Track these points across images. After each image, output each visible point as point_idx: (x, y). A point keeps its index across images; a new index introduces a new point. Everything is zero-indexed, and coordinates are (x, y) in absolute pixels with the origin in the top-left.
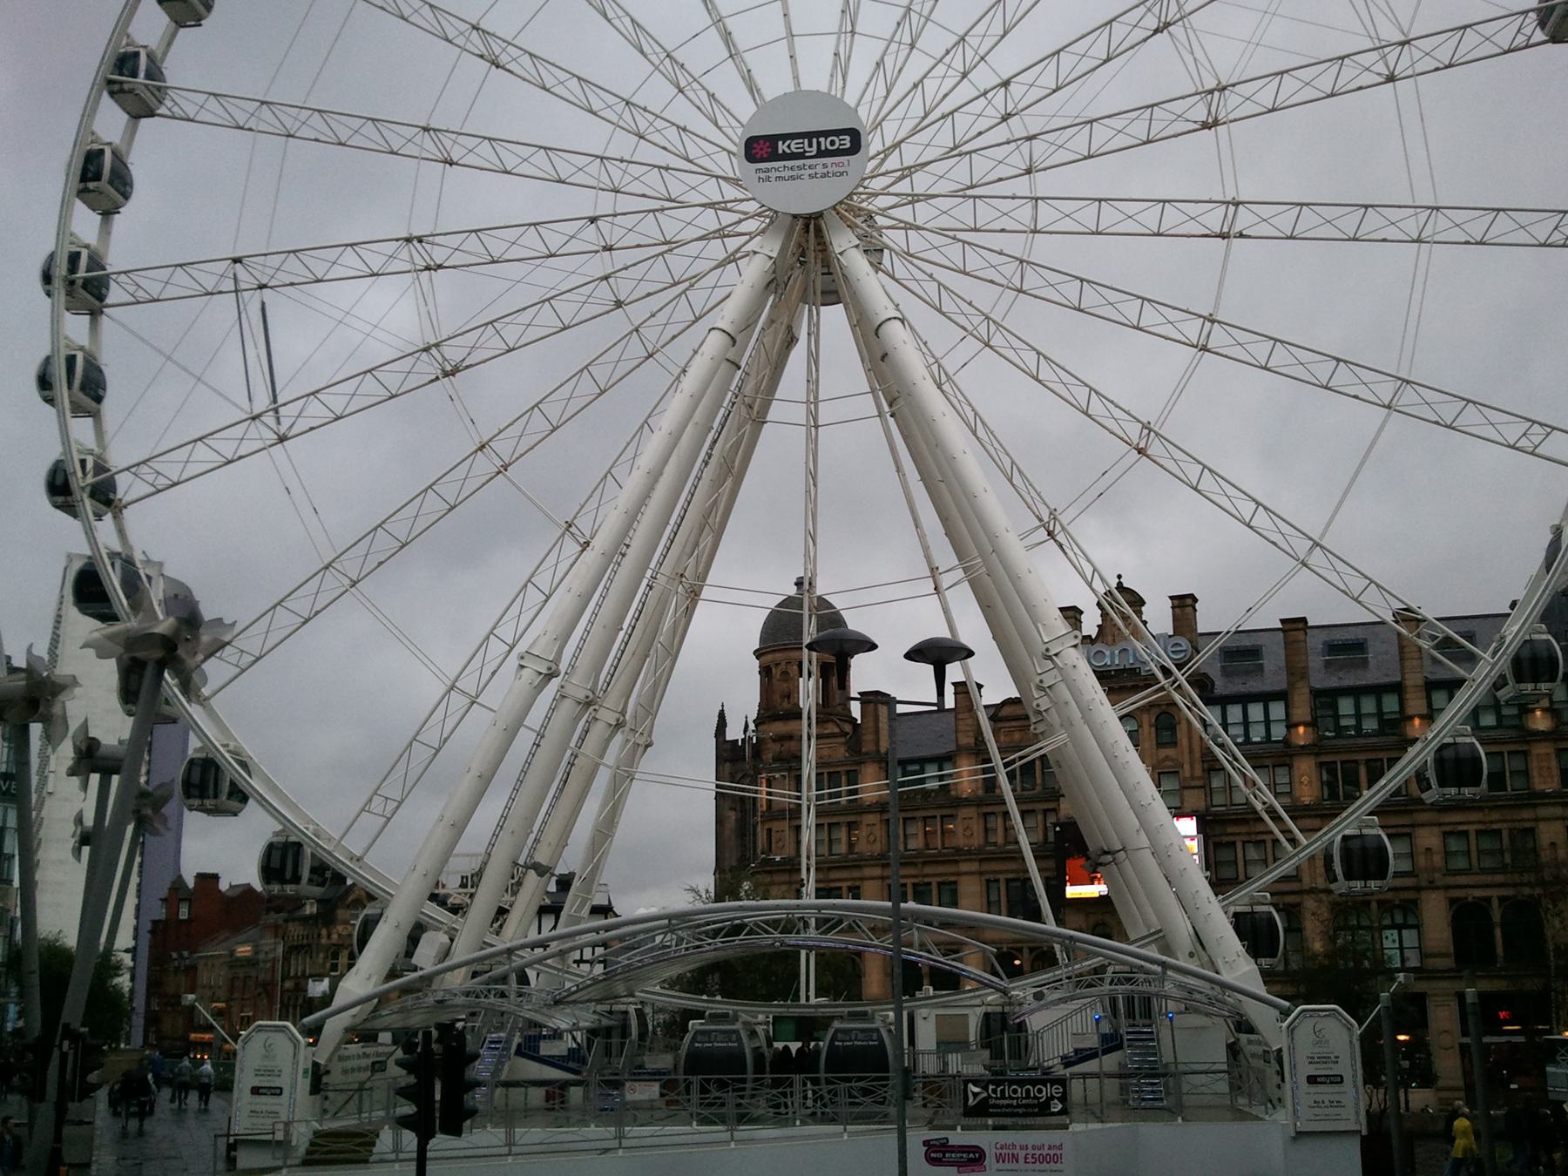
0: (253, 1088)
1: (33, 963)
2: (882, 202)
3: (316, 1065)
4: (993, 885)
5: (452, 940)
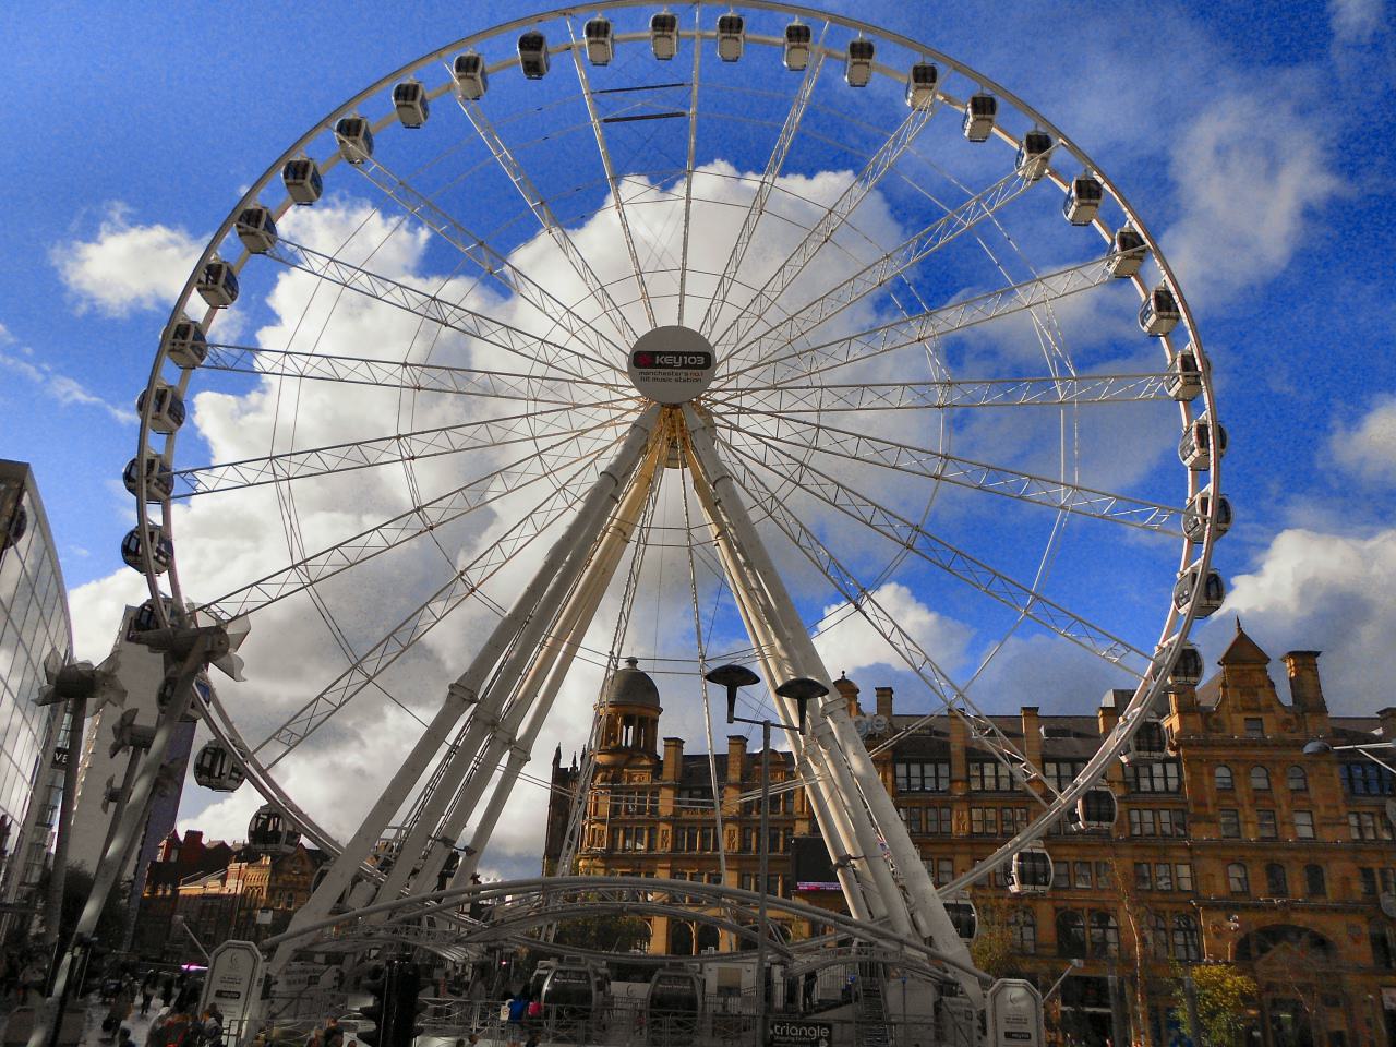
0: (218, 992)
1: (60, 885)
2: (719, 408)
3: (268, 976)
4: (746, 878)
5: (377, 889)
